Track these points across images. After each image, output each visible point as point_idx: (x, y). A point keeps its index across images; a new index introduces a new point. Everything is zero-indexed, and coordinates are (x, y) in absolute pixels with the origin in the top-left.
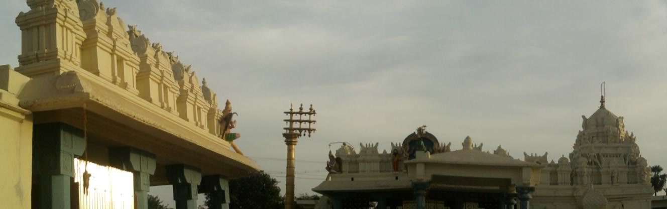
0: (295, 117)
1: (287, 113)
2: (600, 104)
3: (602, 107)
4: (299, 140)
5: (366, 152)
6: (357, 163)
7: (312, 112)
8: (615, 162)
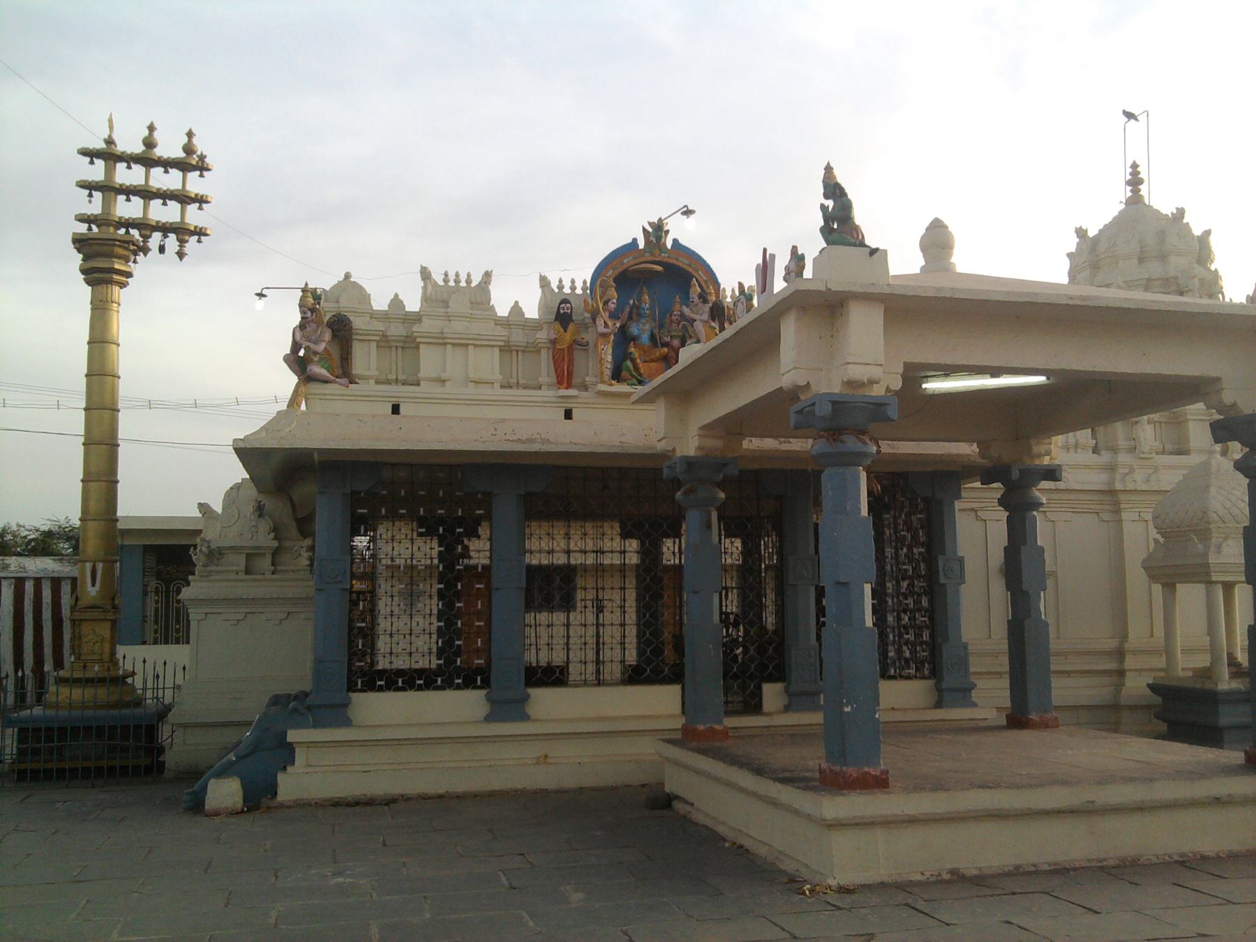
1: (91, 154)
2: (1125, 192)
3: (1135, 200)
4: (144, 269)
5: (445, 303)
6: (410, 344)
7: (191, 162)
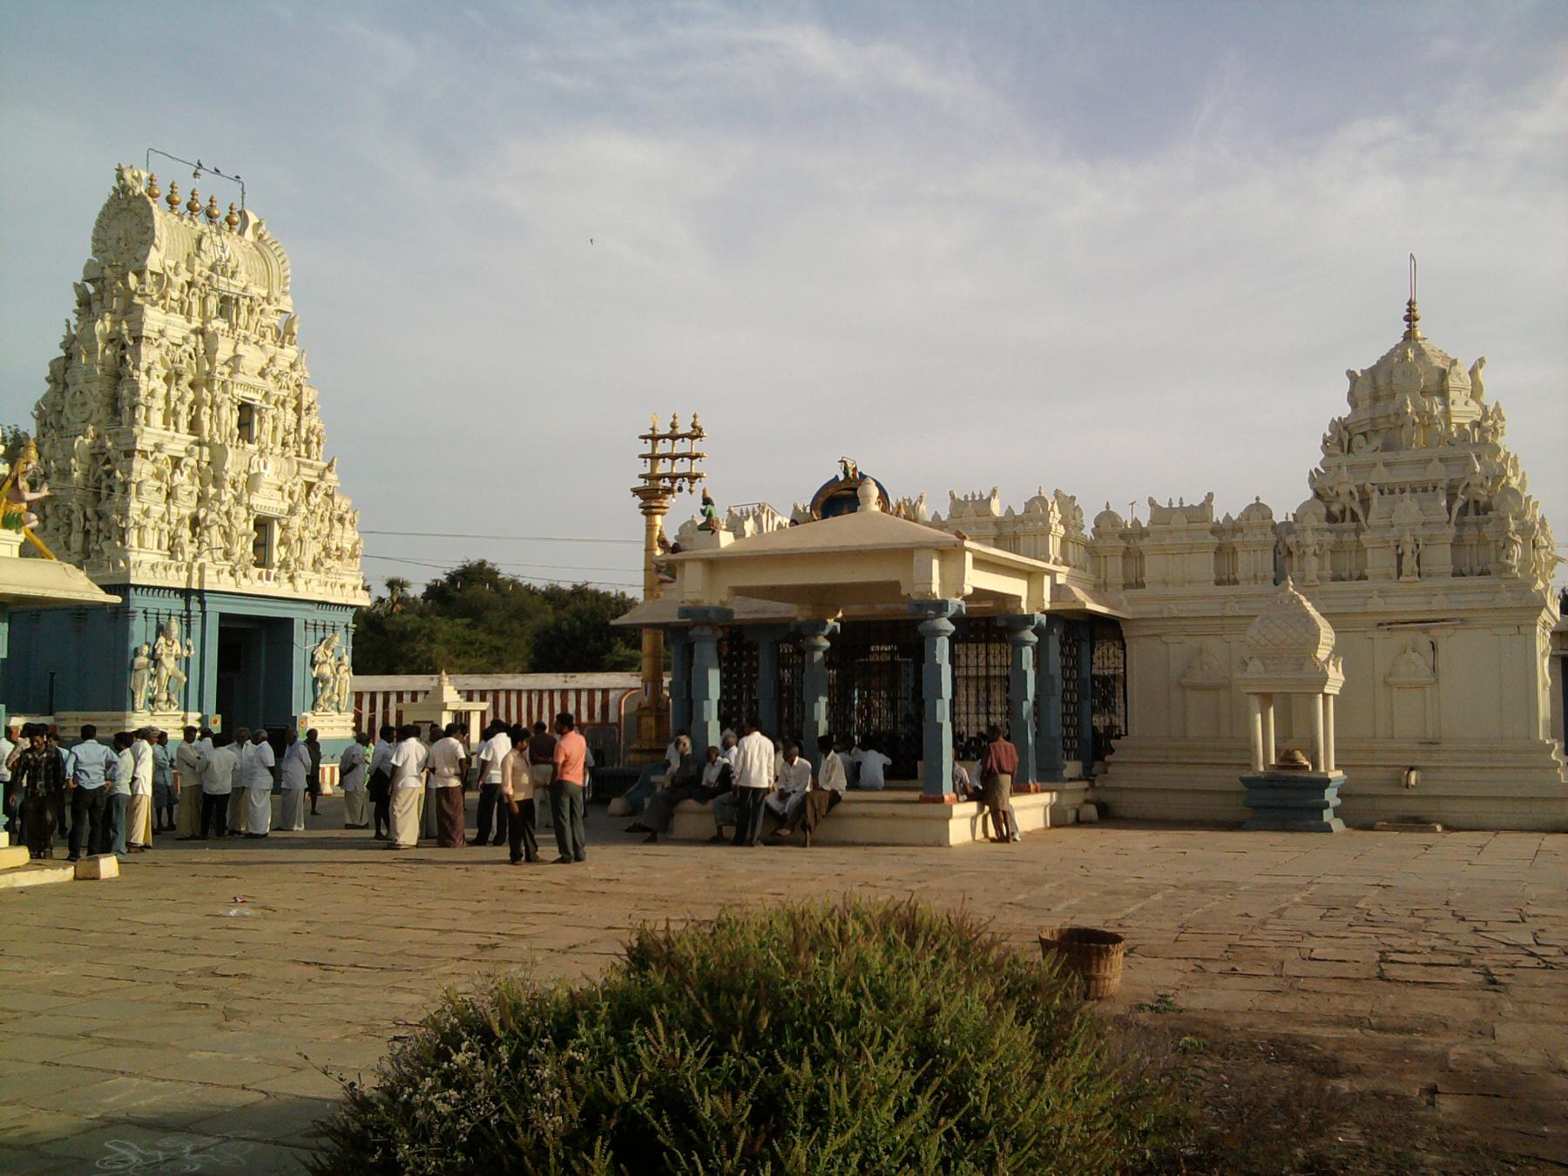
0: (664, 447)
2: (1403, 327)
8: (1408, 509)
